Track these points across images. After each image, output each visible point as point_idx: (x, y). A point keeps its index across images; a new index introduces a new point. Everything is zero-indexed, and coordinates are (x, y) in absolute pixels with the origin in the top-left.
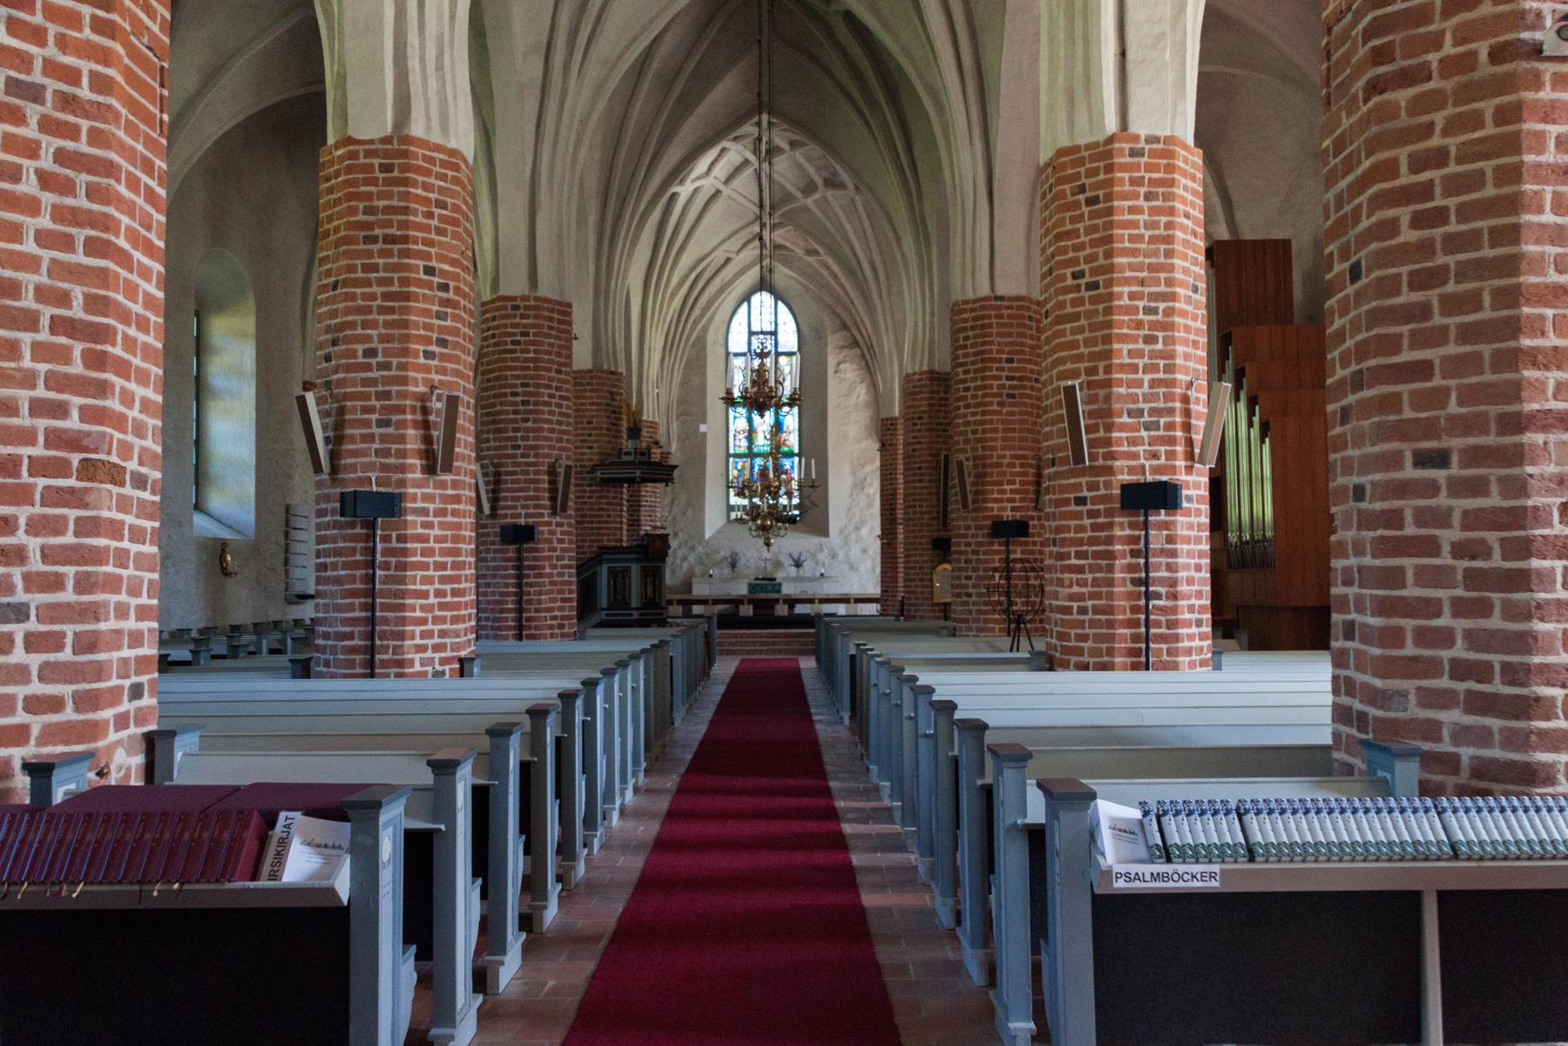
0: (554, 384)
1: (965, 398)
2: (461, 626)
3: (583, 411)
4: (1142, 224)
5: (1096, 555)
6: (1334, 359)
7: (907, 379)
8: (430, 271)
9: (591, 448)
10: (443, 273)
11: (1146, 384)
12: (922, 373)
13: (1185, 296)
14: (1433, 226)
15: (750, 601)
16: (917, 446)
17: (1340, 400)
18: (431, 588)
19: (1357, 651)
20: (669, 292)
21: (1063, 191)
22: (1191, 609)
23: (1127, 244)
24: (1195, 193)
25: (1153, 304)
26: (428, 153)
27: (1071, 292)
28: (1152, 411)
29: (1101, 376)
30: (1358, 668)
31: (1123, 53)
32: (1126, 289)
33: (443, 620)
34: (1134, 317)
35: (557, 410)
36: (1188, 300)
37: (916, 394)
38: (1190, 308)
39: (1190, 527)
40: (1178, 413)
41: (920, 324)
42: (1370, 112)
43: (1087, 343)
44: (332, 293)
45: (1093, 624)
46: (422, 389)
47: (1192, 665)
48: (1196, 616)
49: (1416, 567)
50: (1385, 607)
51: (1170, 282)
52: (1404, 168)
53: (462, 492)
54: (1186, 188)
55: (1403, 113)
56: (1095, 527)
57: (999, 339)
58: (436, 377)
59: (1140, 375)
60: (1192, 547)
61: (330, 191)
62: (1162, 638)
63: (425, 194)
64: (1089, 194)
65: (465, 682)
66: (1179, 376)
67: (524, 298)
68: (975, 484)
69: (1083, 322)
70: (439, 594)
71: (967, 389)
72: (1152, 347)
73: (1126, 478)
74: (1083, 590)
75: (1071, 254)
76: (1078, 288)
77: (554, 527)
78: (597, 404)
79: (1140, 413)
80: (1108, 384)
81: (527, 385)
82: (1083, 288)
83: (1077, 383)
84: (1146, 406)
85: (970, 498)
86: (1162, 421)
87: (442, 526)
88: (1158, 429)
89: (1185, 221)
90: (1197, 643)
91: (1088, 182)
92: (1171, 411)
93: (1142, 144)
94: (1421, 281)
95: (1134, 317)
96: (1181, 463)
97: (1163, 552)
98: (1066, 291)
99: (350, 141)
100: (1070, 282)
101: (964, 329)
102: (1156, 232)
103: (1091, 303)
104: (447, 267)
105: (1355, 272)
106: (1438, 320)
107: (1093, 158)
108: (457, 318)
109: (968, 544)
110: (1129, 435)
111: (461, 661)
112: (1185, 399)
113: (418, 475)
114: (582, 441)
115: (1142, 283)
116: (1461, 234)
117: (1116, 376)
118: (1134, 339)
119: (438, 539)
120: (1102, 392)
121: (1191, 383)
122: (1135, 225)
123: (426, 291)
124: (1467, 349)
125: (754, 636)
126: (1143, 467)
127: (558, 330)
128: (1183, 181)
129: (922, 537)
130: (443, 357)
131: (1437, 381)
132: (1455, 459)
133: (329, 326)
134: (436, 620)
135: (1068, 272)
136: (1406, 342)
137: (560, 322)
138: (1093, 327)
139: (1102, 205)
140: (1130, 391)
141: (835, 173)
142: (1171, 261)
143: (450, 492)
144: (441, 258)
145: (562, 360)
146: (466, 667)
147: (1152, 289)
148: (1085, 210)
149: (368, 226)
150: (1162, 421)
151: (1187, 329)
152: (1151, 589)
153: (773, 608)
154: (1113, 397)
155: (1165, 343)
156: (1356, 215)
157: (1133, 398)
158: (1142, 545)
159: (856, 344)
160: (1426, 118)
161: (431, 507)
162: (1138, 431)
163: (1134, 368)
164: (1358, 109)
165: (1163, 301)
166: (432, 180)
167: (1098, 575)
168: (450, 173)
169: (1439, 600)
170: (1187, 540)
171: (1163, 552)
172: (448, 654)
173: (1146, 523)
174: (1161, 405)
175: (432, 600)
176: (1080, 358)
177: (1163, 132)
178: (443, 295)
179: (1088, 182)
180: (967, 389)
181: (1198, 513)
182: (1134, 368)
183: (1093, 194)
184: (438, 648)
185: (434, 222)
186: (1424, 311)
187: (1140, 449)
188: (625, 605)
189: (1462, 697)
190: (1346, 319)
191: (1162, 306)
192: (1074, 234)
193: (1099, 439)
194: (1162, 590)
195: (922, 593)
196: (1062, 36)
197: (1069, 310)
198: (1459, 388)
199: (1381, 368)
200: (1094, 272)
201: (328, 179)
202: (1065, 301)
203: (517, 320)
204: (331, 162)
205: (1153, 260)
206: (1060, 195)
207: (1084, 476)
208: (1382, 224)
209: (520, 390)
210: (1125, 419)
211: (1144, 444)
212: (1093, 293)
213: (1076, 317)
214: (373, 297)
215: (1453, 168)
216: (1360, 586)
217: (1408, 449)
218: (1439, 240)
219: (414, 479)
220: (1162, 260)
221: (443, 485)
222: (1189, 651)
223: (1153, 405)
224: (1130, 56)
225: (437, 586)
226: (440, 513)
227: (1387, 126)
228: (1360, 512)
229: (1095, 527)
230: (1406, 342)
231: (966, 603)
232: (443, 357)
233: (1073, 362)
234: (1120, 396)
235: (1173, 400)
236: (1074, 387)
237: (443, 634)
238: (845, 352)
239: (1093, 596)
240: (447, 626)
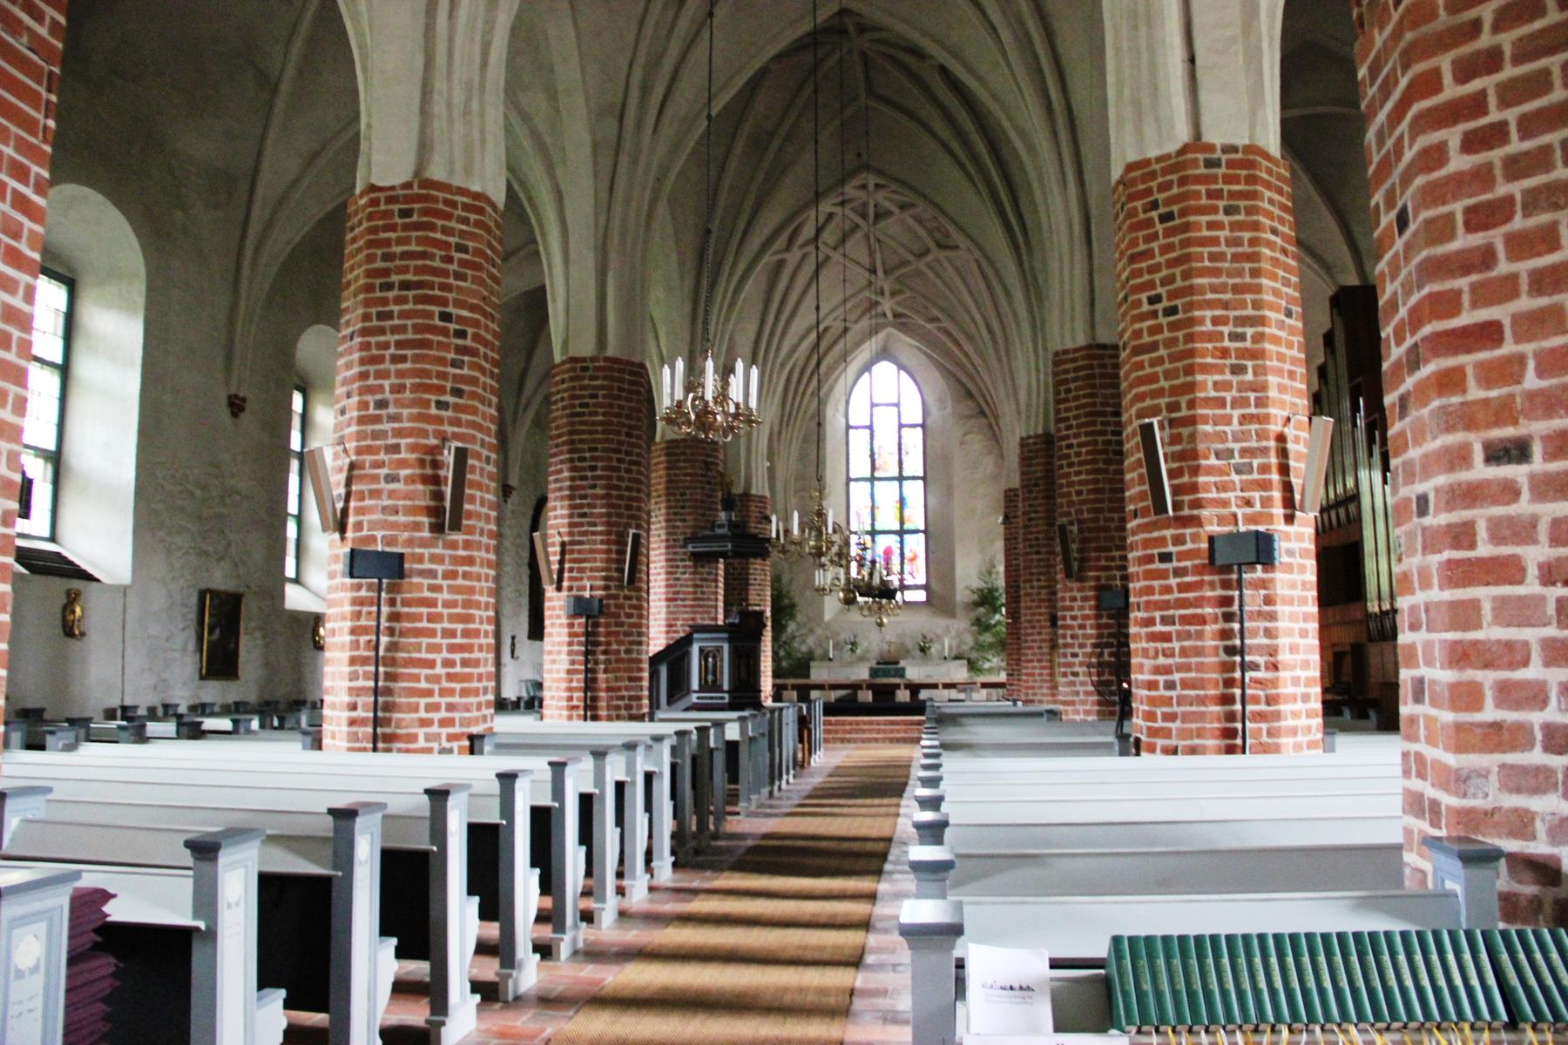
0: (623, 448)
1: (1068, 456)
2: (473, 700)
3: (677, 482)
4: (1222, 240)
5: (1185, 620)
6: (1388, 336)
7: (1023, 443)
8: (446, 317)
9: (685, 521)
10: (461, 320)
11: (1235, 420)
12: (1037, 436)
13: (1277, 321)
14: (1491, 148)
15: (870, 686)
16: (1033, 515)
17: (1397, 388)
18: (438, 658)
19: (1427, 718)
20: (779, 361)
21: (1135, 208)
22: (1296, 681)
23: (1207, 263)
24: (1283, 208)
25: (1240, 330)
26: (449, 196)
27: (1148, 319)
28: (1245, 452)
29: (1184, 413)
30: (1431, 741)
31: (1192, 60)
32: (1208, 314)
33: (451, 692)
34: (1218, 345)
35: (626, 476)
36: (1281, 325)
37: (1031, 458)
38: (1283, 334)
39: (1293, 586)
40: (1273, 453)
41: (1034, 385)
42: (1402, 17)
43: (1168, 375)
44: (349, 343)
45: (1181, 700)
46: (433, 441)
47: (1297, 747)
48: (1301, 690)
49: (1494, 599)
50: (1461, 656)
51: (1257, 305)
52: (1447, 78)
53: (475, 553)
54: (1271, 201)
55: (1442, 12)
56: (1183, 588)
57: (1104, 391)
58: (449, 429)
59: (1228, 410)
60: (1295, 608)
61: (354, 240)
62: (1261, 717)
63: (444, 238)
64: (1162, 210)
65: (475, 759)
66: (1272, 411)
67: (593, 359)
68: (1081, 551)
69: (1162, 352)
70: (448, 663)
71: (1070, 446)
72: (1241, 378)
73: (1214, 528)
74: (1170, 661)
75: (1146, 277)
76: (1154, 314)
77: (621, 601)
78: (690, 475)
79: (1230, 453)
80: (1192, 421)
81: (595, 449)
82: (1160, 313)
83: (1155, 421)
84: (1236, 446)
85: (1075, 565)
86: (1256, 463)
87: (452, 589)
88: (1251, 471)
89: (1273, 238)
90: (1303, 722)
91: (1161, 197)
92: (1264, 451)
93: (1218, 154)
94: (1479, 218)
95: (1218, 345)
96: (1278, 511)
97: (1260, 615)
98: (1142, 317)
99: (373, 188)
100: (1146, 307)
101: (1066, 381)
102: (1240, 250)
103: (1169, 330)
104: (465, 313)
105: (1402, 221)
106: (1504, 267)
107: (1165, 171)
108: (473, 366)
109: (1074, 618)
110: (1218, 479)
111: (471, 738)
112: (1281, 438)
113: (426, 534)
114: (675, 514)
115: (1226, 305)
116: (1527, 154)
117: (1200, 411)
118: (1219, 369)
119: (447, 604)
120: (1185, 431)
121: (1288, 419)
122: (1214, 241)
123: (441, 338)
124: (1543, 301)
125: (871, 723)
126: (1235, 516)
127: (631, 392)
128: (1268, 194)
129: (1040, 614)
130: (457, 408)
131: (1509, 348)
132: (1537, 450)
133: (345, 378)
134: (444, 692)
135: (1144, 297)
136: (1466, 299)
137: (631, 383)
138: (1173, 358)
139: (1177, 222)
140: (1219, 428)
141: (947, 235)
142: (1257, 281)
143: (462, 553)
144: (459, 304)
145: (633, 423)
146: (477, 743)
147: (1237, 313)
148: (1159, 227)
149: (385, 272)
150: (1256, 463)
151: (1281, 357)
152: (1247, 658)
153: (893, 694)
154: (1199, 437)
155: (1255, 374)
156: (1398, 150)
157: (1222, 437)
158: (1236, 607)
159: (982, 413)
160: (1470, 14)
161: (440, 569)
162: (1228, 474)
163: (1221, 403)
164: (1389, 17)
165: (1251, 326)
166: (453, 224)
167: (1186, 643)
168: (473, 217)
169: (1526, 644)
170: (1289, 601)
171: (1260, 615)
172: (457, 729)
173: (1240, 580)
174: (1254, 444)
175: (439, 670)
176: (1159, 393)
177: (1242, 140)
178: (460, 342)
179: (1161, 197)
180: (1070, 446)
181: (1302, 569)
182: (1221, 403)
183: (1167, 210)
184: (444, 723)
185: (453, 267)
186: (1486, 257)
187: (1231, 495)
188: (716, 687)
189: (1560, 776)
190: (1397, 283)
191: (1249, 331)
192: (1148, 254)
193: (1183, 485)
194: (1261, 660)
195: (1040, 675)
196: (1125, 45)
197: (1146, 339)
198: (1537, 355)
199: (1437, 336)
200: (1172, 295)
201: (352, 229)
202: (1141, 330)
203: (586, 382)
204: (356, 212)
205: (1238, 280)
206: (1133, 213)
207: (1168, 527)
208: (1425, 152)
209: (587, 455)
210: (1213, 461)
211: (1235, 490)
212: (1172, 318)
213: (1154, 347)
214: (386, 346)
215: (1509, 72)
216: (1428, 630)
217: (1476, 441)
218: (1498, 165)
219: (422, 538)
220: (1247, 280)
221: (453, 545)
222: (1293, 732)
223: (1244, 445)
224: (1199, 61)
225: (445, 654)
226: (449, 575)
227: (1424, 29)
228: (1424, 529)
229: (1183, 588)
230: (1466, 299)
231: (1072, 684)
232: (457, 408)
233: (1152, 398)
234: (1206, 434)
235: (1267, 439)
236: (1151, 425)
237: (451, 707)
238: (973, 421)
239: (1182, 668)
240: (456, 699)
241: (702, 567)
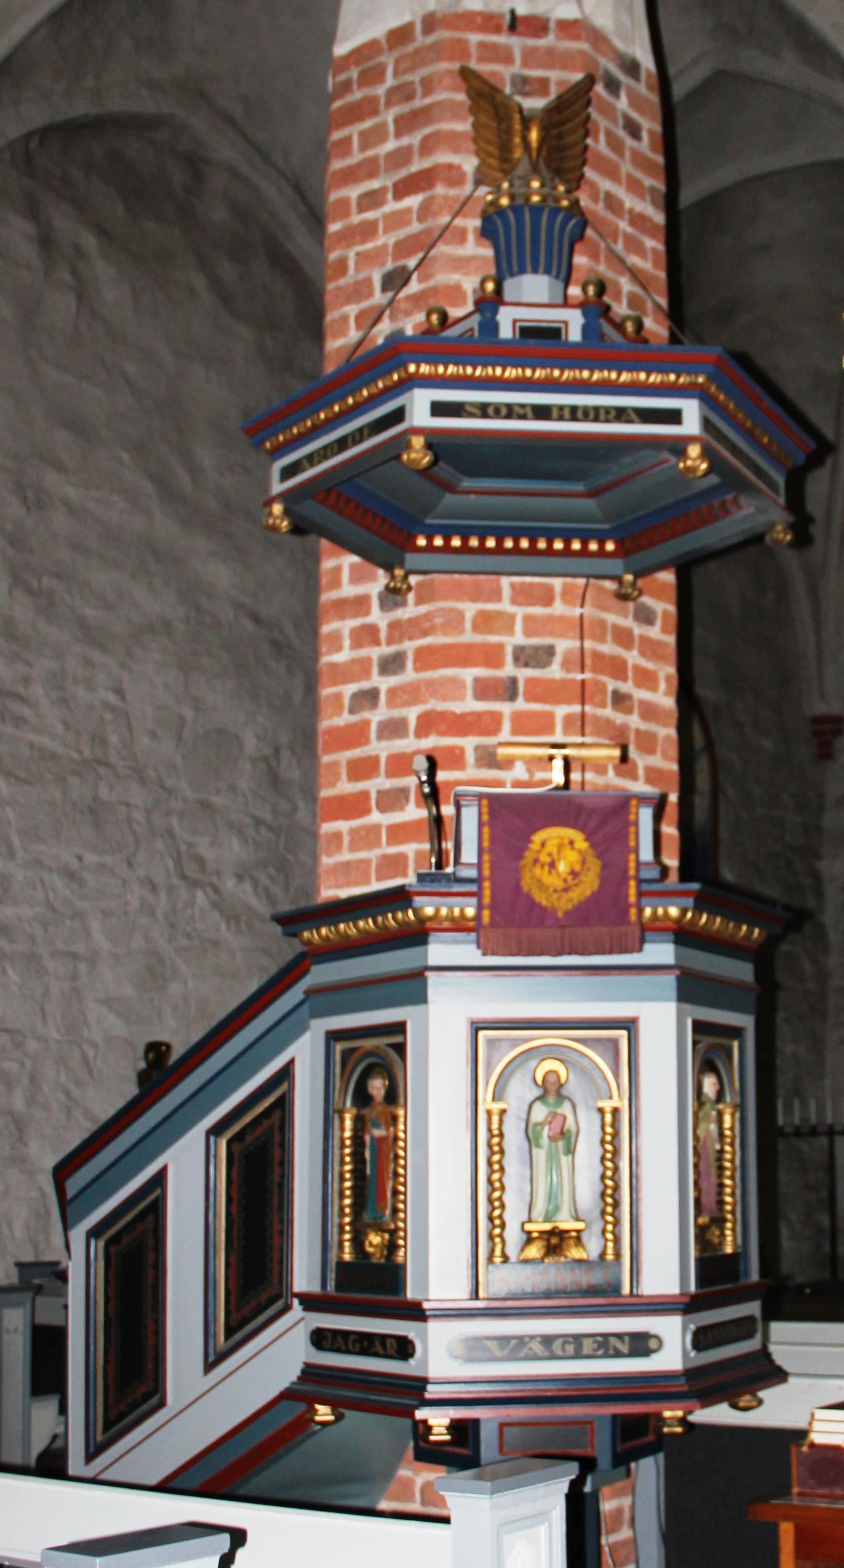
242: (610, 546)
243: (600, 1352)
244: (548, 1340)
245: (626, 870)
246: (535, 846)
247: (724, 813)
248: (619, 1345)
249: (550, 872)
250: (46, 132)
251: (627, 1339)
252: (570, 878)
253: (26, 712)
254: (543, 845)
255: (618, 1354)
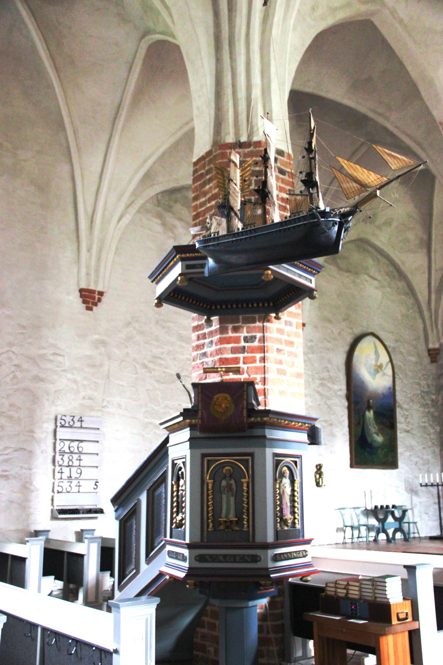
241: (236, 329)
242: (271, 304)
243: (242, 561)
244: (225, 556)
245: (243, 405)
246: (215, 400)
247: (397, 382)
248: (247, 559)
249: (220, 407)
250: (163, 192)
251: (250, 556)
252: (226, 409)
253: (163, 363)
254: (218, 399)
255: (247, 562)
